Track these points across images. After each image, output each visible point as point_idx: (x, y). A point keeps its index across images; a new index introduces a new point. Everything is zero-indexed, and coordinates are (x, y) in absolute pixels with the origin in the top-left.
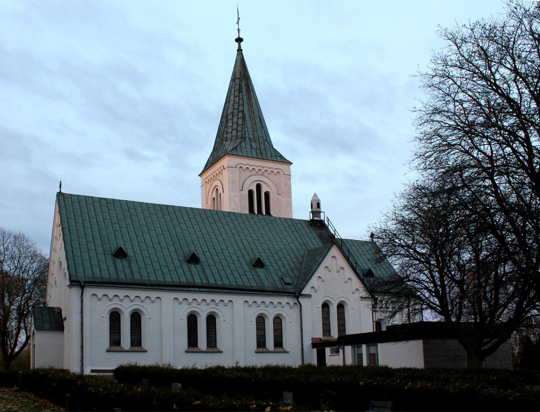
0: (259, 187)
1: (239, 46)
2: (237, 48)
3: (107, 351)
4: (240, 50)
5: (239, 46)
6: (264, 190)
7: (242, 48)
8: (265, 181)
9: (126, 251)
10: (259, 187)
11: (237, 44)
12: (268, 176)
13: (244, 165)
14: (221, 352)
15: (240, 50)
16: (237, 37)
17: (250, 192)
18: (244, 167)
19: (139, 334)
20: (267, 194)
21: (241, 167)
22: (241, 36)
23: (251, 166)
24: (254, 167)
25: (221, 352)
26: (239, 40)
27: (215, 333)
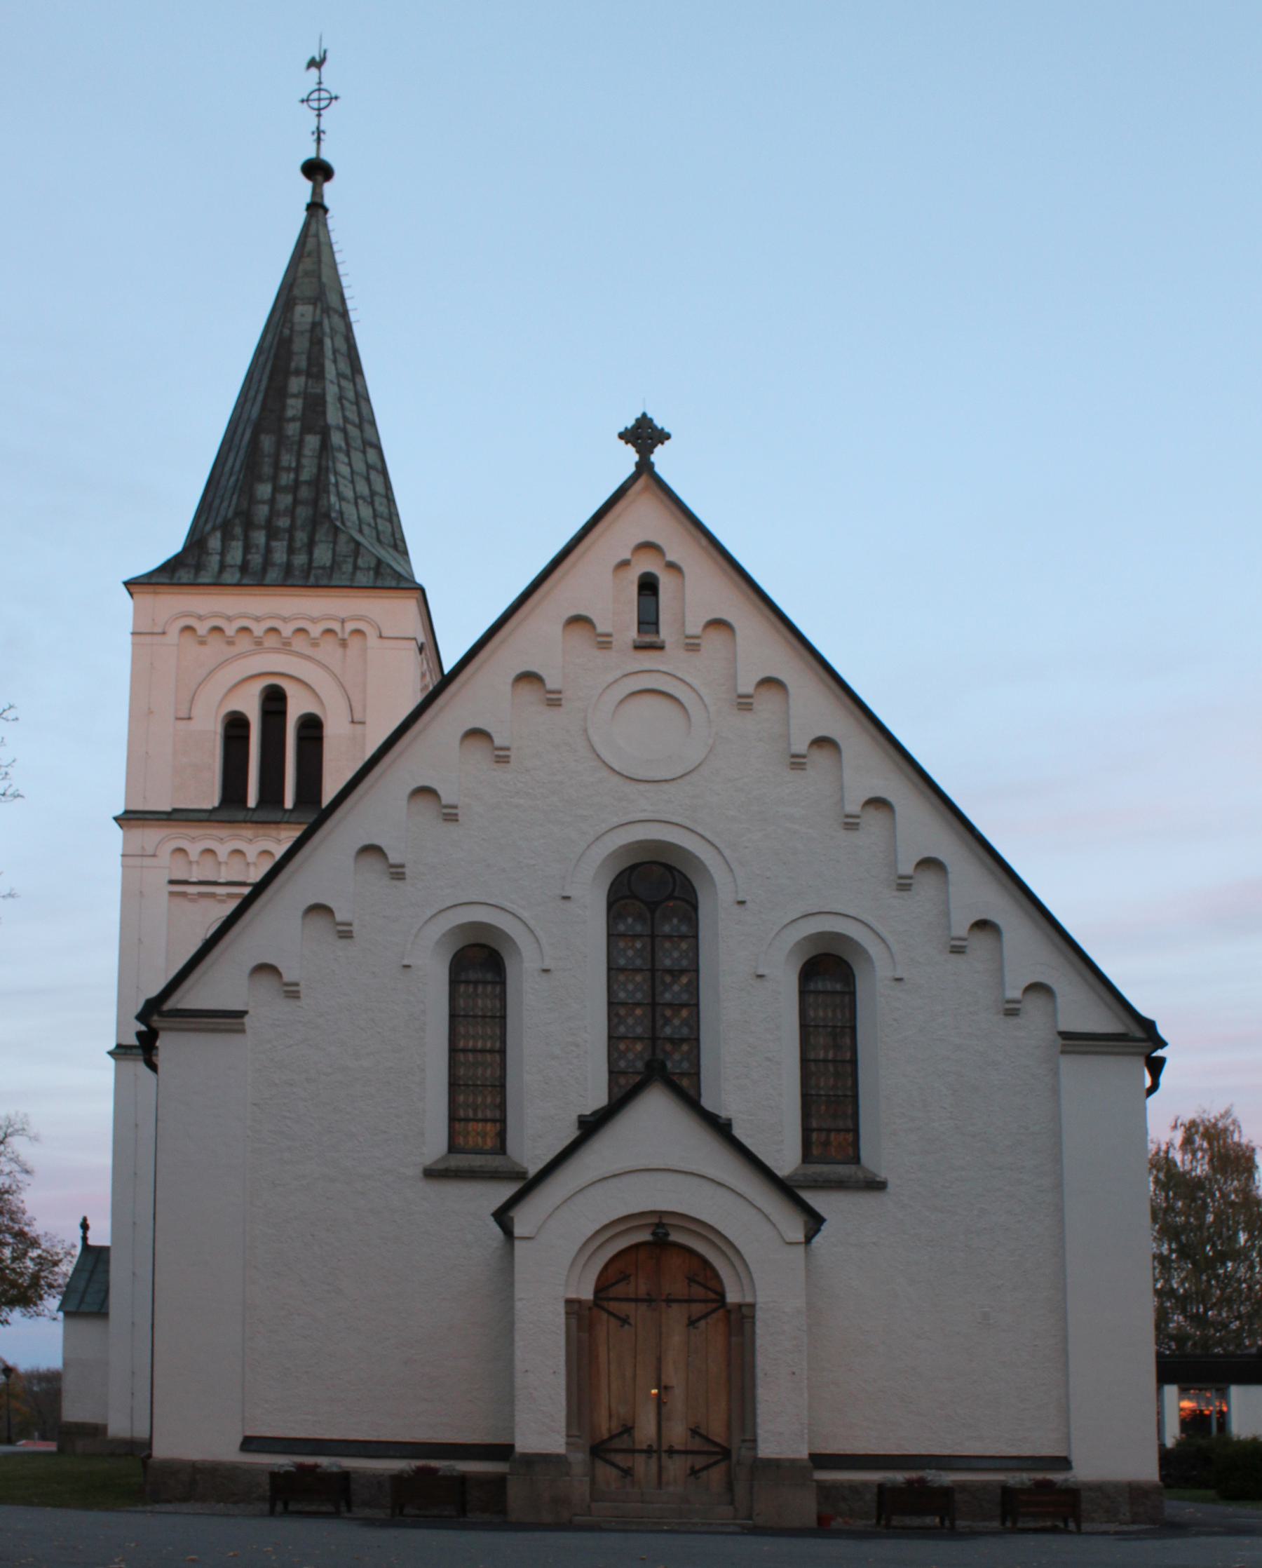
0: (274, 700)
1: (317, 193)
2: (307, 198)
3: (431, 1174)
4: (316, 208)
5: (317, 193)
6: (295, 710)
7: (327, 202)
8: (306, 680)
9: (216, 920)
10: (274, 700)
11: (307, 185)
12: (308, 651)
13: (285, 620)
14: (876, 1185)
15: (316, 208)
16: (312, 155)
17: (235, 727)
18: (202, 628)
19: (849, 1068)
20: (312, 728)
21: (188, 629)
22: (326, 156)
23: (314, 620)
24: (218, 622)
25: (876, 1185)
26: (317, 170)
27: (850, 1124)
